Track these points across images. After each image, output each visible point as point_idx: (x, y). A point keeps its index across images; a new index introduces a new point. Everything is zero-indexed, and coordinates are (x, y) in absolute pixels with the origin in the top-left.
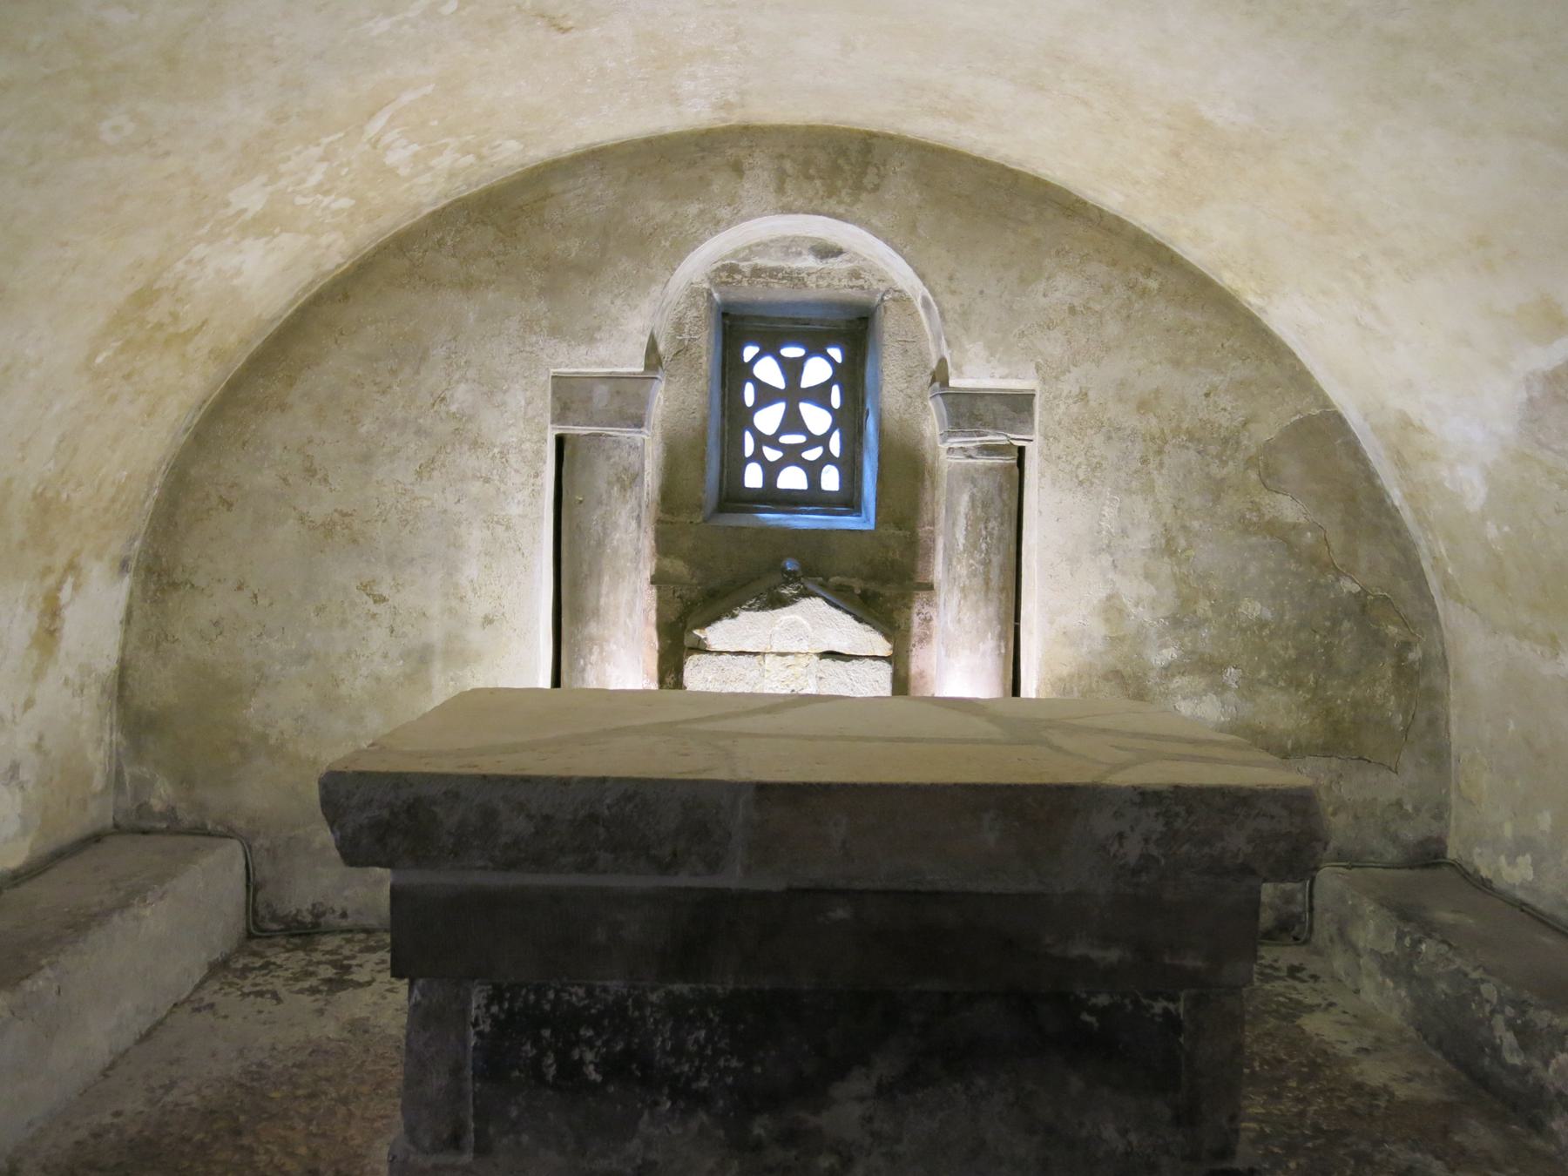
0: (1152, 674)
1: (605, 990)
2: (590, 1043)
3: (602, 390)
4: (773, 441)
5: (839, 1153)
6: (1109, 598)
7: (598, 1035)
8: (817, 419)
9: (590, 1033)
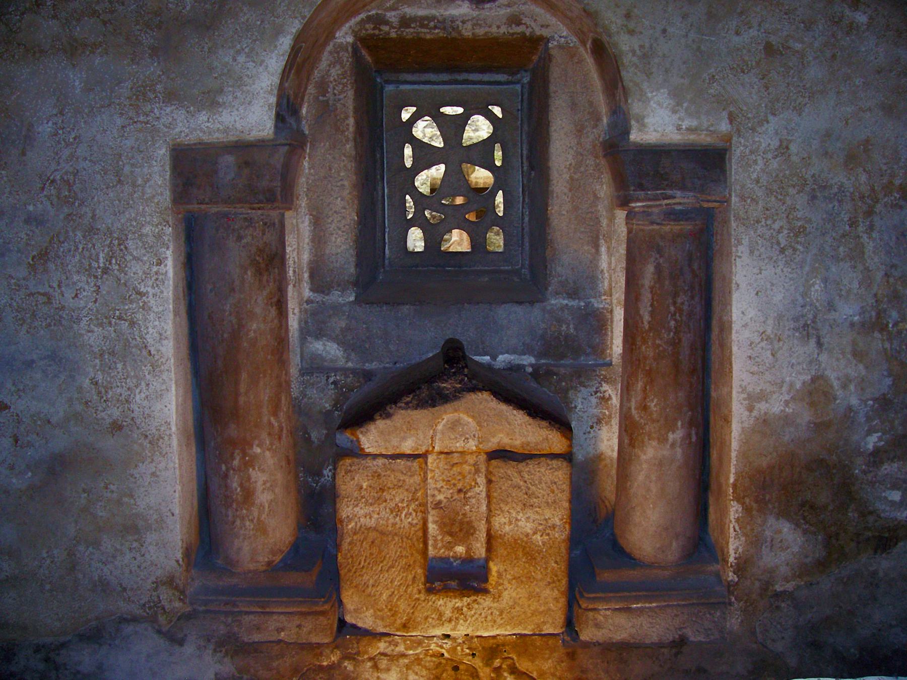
0: (859, 461)
6: (814, 380)
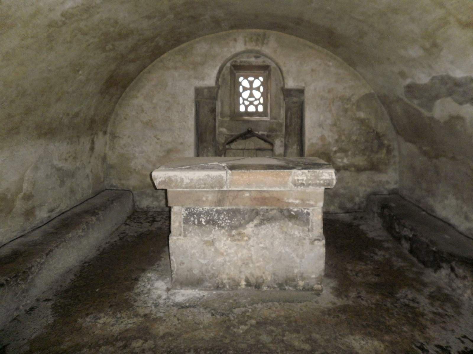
1: (205, 208)
2: (203, 218)
3: (206, 90)
4: (247, 100)
5: (248, 237)
7: (204, 216)
8: (257, 94)
9: (203, 216)
